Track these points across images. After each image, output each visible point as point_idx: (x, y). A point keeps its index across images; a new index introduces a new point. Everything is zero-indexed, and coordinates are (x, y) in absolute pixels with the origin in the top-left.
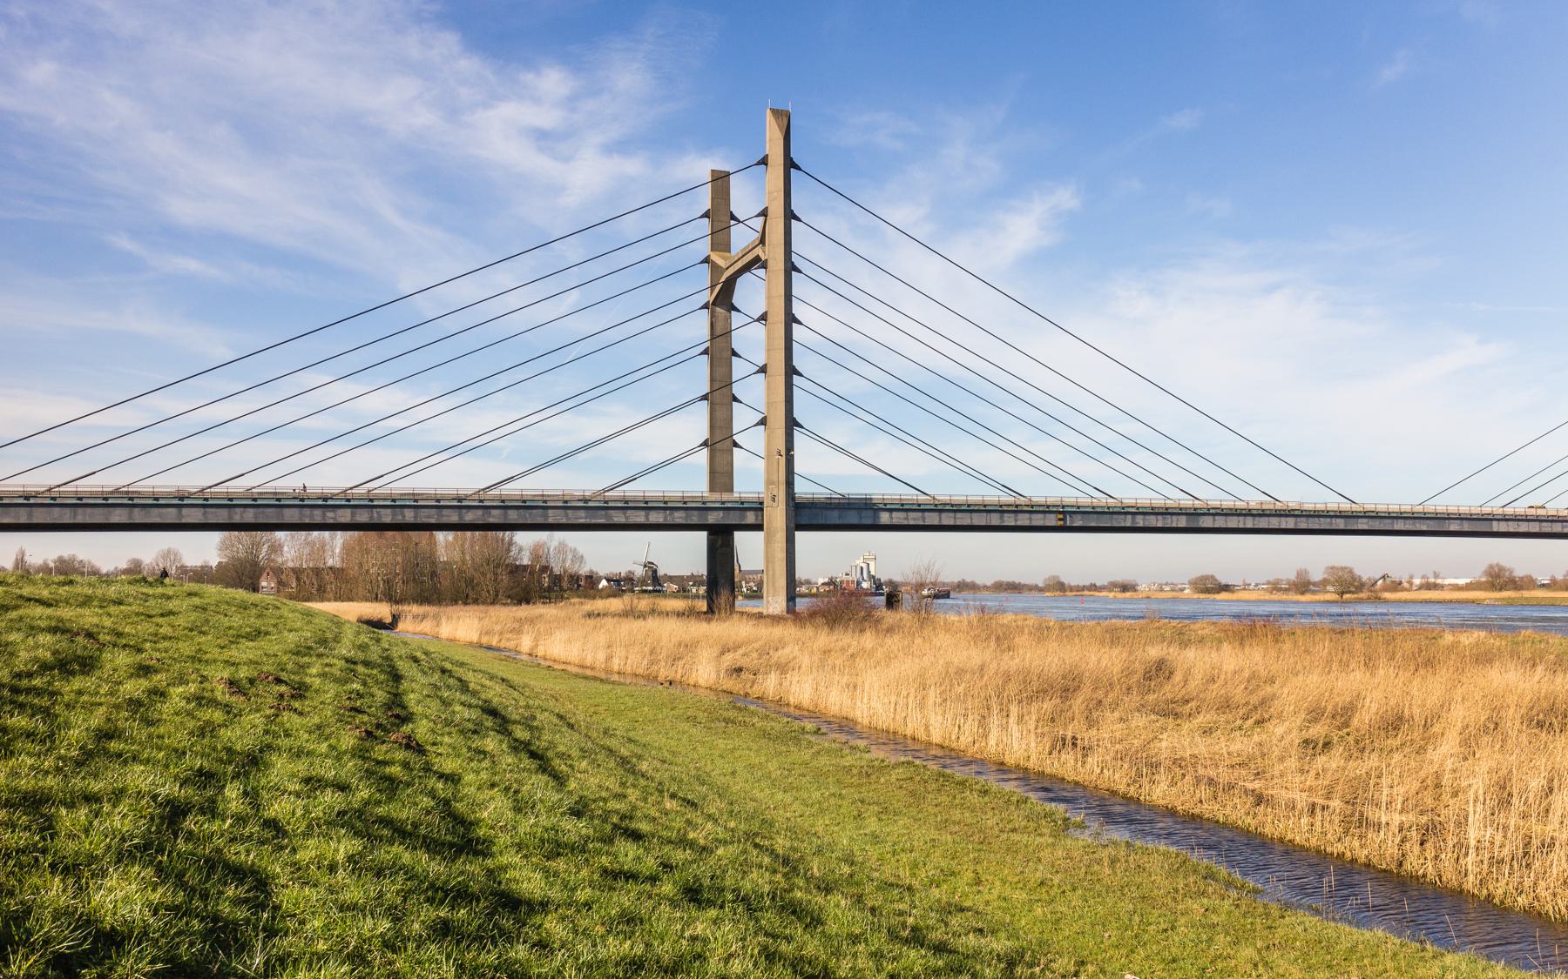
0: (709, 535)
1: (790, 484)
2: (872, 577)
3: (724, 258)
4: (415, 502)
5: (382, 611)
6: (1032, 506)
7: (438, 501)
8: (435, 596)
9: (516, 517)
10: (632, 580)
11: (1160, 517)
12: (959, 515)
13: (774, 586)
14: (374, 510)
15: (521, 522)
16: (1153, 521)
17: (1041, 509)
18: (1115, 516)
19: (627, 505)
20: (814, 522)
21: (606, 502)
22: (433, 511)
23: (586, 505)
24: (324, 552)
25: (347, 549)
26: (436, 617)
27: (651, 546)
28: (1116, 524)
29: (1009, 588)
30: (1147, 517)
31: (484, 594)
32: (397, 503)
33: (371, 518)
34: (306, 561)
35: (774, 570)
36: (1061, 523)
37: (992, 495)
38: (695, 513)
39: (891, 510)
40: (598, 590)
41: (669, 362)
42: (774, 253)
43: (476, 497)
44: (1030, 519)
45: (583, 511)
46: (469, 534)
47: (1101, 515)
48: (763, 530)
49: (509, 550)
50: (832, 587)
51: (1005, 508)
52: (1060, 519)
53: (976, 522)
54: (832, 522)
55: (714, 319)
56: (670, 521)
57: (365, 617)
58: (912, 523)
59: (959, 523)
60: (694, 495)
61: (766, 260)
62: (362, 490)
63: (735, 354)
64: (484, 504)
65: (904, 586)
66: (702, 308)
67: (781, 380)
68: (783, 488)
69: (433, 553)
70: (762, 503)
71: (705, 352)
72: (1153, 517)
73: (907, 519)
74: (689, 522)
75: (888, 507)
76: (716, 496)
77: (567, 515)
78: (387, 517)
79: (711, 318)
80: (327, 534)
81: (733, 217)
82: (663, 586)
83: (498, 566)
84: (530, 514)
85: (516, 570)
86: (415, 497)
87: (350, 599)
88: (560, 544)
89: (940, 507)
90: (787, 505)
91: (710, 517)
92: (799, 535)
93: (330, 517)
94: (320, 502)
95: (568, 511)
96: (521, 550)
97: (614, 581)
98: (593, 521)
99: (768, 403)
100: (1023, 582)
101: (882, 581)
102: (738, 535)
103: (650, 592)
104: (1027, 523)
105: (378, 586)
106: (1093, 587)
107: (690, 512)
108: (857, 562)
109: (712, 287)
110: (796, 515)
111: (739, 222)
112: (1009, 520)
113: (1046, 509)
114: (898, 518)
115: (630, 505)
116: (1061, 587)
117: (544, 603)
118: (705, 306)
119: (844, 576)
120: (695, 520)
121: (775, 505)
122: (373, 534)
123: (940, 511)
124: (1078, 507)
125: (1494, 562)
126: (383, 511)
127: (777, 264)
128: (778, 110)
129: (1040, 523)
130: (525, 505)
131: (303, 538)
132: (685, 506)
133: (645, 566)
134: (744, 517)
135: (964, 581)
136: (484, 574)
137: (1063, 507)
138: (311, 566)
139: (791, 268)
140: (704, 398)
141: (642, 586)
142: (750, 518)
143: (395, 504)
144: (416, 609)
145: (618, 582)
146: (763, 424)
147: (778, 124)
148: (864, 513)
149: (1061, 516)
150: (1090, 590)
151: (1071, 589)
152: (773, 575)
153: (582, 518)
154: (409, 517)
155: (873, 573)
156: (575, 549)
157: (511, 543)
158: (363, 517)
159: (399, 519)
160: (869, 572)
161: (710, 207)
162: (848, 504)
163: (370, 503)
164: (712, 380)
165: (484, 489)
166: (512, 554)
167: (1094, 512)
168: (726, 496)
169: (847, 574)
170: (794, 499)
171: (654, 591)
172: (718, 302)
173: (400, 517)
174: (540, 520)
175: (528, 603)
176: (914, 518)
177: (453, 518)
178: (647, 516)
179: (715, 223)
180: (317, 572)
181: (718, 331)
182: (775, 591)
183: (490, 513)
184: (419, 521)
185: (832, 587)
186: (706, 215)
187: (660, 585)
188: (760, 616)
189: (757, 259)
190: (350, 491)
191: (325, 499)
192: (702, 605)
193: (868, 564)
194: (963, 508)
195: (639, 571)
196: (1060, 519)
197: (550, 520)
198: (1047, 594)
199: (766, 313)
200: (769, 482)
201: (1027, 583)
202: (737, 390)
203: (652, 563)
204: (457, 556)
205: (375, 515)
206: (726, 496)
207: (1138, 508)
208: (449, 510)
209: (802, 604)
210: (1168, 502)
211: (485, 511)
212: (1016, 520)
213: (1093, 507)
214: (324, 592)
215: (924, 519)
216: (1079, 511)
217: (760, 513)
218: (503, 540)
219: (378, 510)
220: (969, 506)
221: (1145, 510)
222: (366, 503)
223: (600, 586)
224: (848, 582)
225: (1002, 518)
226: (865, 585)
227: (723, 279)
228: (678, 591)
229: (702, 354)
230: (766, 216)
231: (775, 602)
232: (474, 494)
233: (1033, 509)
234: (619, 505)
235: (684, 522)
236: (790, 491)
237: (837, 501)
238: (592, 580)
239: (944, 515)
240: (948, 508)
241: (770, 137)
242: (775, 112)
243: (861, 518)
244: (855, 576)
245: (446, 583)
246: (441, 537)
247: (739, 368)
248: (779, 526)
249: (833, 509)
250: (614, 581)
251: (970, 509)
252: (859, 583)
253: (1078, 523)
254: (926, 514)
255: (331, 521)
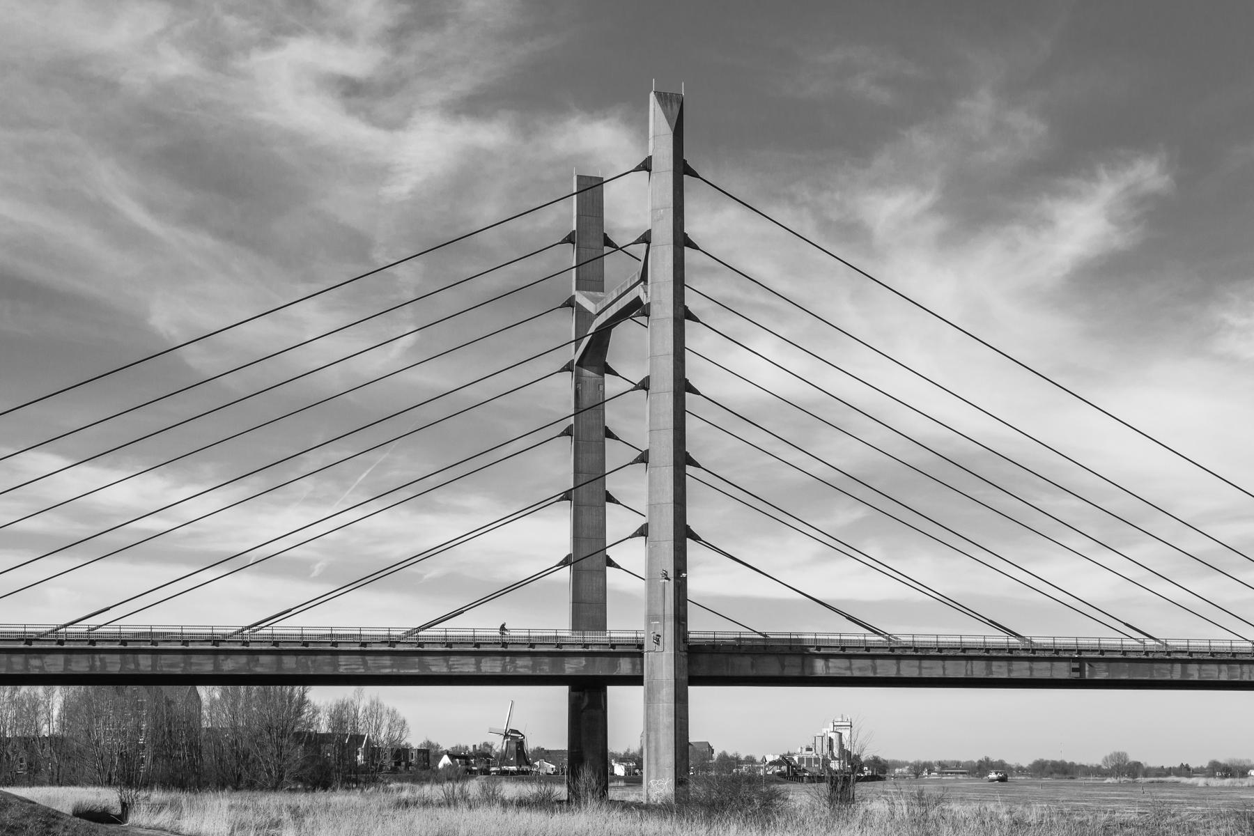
0: (571, 691)
1: (680, 618)
2: (845, 754)
3: (595, 300)
4: (152, 643)
5: (108, 797)
6: (1034, 651)
7: (185, 642)
8: (193, 779)
9: (294, 666)
10: (488, 755)
11: (1224, 667)
12: (926, 663)
13: (657, 764)
14: (97, 656)
15: (300, 672)
16: (1212, 672)
17: (1047, 654)
18: (1156, 666)
19: (450, 648)
20: (716, 673)
21: (421, 645)
22: (179, 657)
23: (392, 648)
24: (36, 714)
25: (69, 711)
26: (175, 806)
27: (515, 706)
28: (1157, 677)
29: (1056, 772)
30: (1204, 667)
31: (264, 775)
32: (128, 647)
33: (92, 667)
34: (10, 729)
35: (657, 742)
36: (1077, 675)
37: (976, 634)
38: (547, 660)
39: (826, 657)
40: (438, 771)
41: (537, 437)
42: (660, 295)
43: (238, 638)
44: (1031, 669)
45: (388, 658)
46: (242, 689)
47: (1134, 664)
48: (642, 685)
49: (299, 712)
50: (784, 768)
51: (995, 654)
52: (1074, 670)
53: (881, 673)
54: (742, 673)
55: (579, 385)
56: (510, 671)
57: (86, 807)
58: (857, 674)
59: (926, 674)
60: (544, 634)
61: (649, 304)
62: (81, 628)
63: (609, 434)
64: (250, 648)
65: (899, 767)
66: (563, 370)
67: (668, 473)
68: (670, 625)
69: (195, 717)
70: (641, 646)
71: (567, 432)
72: (1214, 667)
73: (850, 668)
74: (538, 673)
75: (822, 651)
76: (578, 637)
77: (365, 663)
78: (114, 665)
79: (576, 384)
80: (40, 690)
81: (608, 242)
82: (531, 765)
83: (283, 734)
84: (313, 662)
85: (315, 741)
86: (152, 637)
87: (73, 783)
88: (372, 703)
89: (898, 652)
90: (676, 648)
91: (567, 666)
92: (693, 691)
93: (35, 665)
94: (22, 645)
95: (367, 658)
96: (316, 711)
97: (460, 757)
98: (402, 672)
99: (650, 505)
100: (1077, 762)
101: (863, 759)
102: (612, 690)
103: (512, 773)
104: (1025, 675)
105: (113, 763)
106: (1185, 771)
107: (538, 659)
108: (824, 731)
109: (578, 341)
110: (689, 664)
111: (617, 248)
112: (1000, 671)
113: (1055, 655)
114: (837, 668)
115: (455, 648)
116: (1134, 770)
117: (348, 789)
118: (568, 368)
119: (804, 750)
120: (546, 669)
121: (659, 648)
122: (108, 690)
123: (899, 658)
124: (1102, 652)
125: (1120, 749)
126: (109, 658)
127: (663, 310)
128: (665, 93)
129: (1046, 675)
130: (306, 648)
131: (7, 694)
132: (532, 649)
133: (506, 736)
134: (615, 666)
135: (987, 759)
136: (263, 747)
137: (1080, 652)
138: (18, 734)
139: (683, 315)
140: (566, 496)
141: (501, 765)
142: (625, 667)
143: (127, 646)
144: (157, 796)
145: (466, 758)
146: (642, 535)
147: (667, 117)
148: (788, 660)
149: (1076, 665)
150: (1178, 775)
151: (1147, 772)
152: (657, 750)
153: (385, 667)
154: (145, 664)
155: (847, 747)
156: (394, 712)
157: (302, 702)
158: (80, 666)
159: (131, 668)
160: (841, 745)
161: (575, 228)
162: (765, 647)
163: (91, 647)
164: (577, 472)
165: (249, 627)
166: (304, 717)
167: (1124, 658)
168: (590, 637)
169: (809, 749)
170: (685, 639)
171: (518, 772)
172: (585, 361)
173: (132, 666)
174: (327, 670)
175: (325, 788)
176: (860, 668)
177: (229, 666)
178: (478, 664)
179: (582, 251)
180: (28, 743)
181: (586, 401)
182: (658, 771)
183: (258, 660)
184: (158, 671)
185: (784, 768)
186: (570, 239)
187: (528, 763)
188: (639, 806)
189: (637, 303)
190: (63, 630)
191: (29, 641)
192: (561, 791)
193: (841, 734)
194: (932, 653)
195: (499, 744)
196: (1074, 670)
197: (342, 670)
198: (1109, 780)
199: (648, 378)
200: (651, 617)
201: (1085, 763)
202: (611, 485)
203: (517, 732)
204: (224, 720)
205: (98, 663)
206: (590, 637)
207: (1191, 654)
208: (201, 657)
209: (697, 790)
210: (1150, 642)
211: (250, 657)
212: (1010, 671)
213: (1124, 653)
214: (36, 772)
215: (874, 669)
216: (1103, 656)
217: (638, 660)
218: (291, 697)
219: (102, 656)
220: (940, 650)
221: (1200, 657)
222: (85, 646)
223: (441, 765)
224: (809, 760)
225: (989, 668)
226: (835, 765)
227: (592, 330)
228: (555, 773)
229: (562, 434)
230: (648, 243)
231: (659, 785)
232: (235, 633)
233: (1034, 654)
234: (439, 648)
235: (530, 673)
236: (681, 630)
237: (749, 643)
238: (428, 754)
239: (904, 663)
240: (909, 652)
241: (654, 132)
242: (663, 98)
243: (783, 667)
244: (821, 751)
245: (208, 759)
246: (203, 691)
247: (615, 453)
248: (664, 678)
249: (743, 654)
250: (460, 757)
251: (941, 654)
252: (826, 762)
253: (1102, 675)
254: (879, 662)
255: (36, 672)
